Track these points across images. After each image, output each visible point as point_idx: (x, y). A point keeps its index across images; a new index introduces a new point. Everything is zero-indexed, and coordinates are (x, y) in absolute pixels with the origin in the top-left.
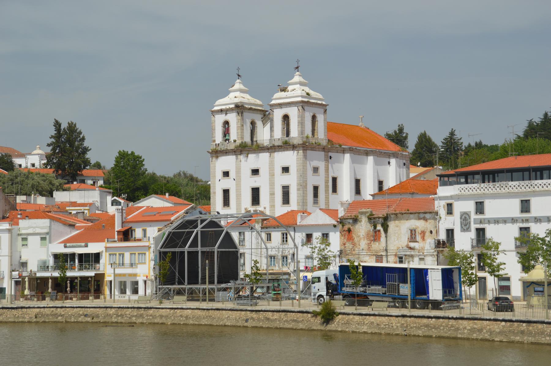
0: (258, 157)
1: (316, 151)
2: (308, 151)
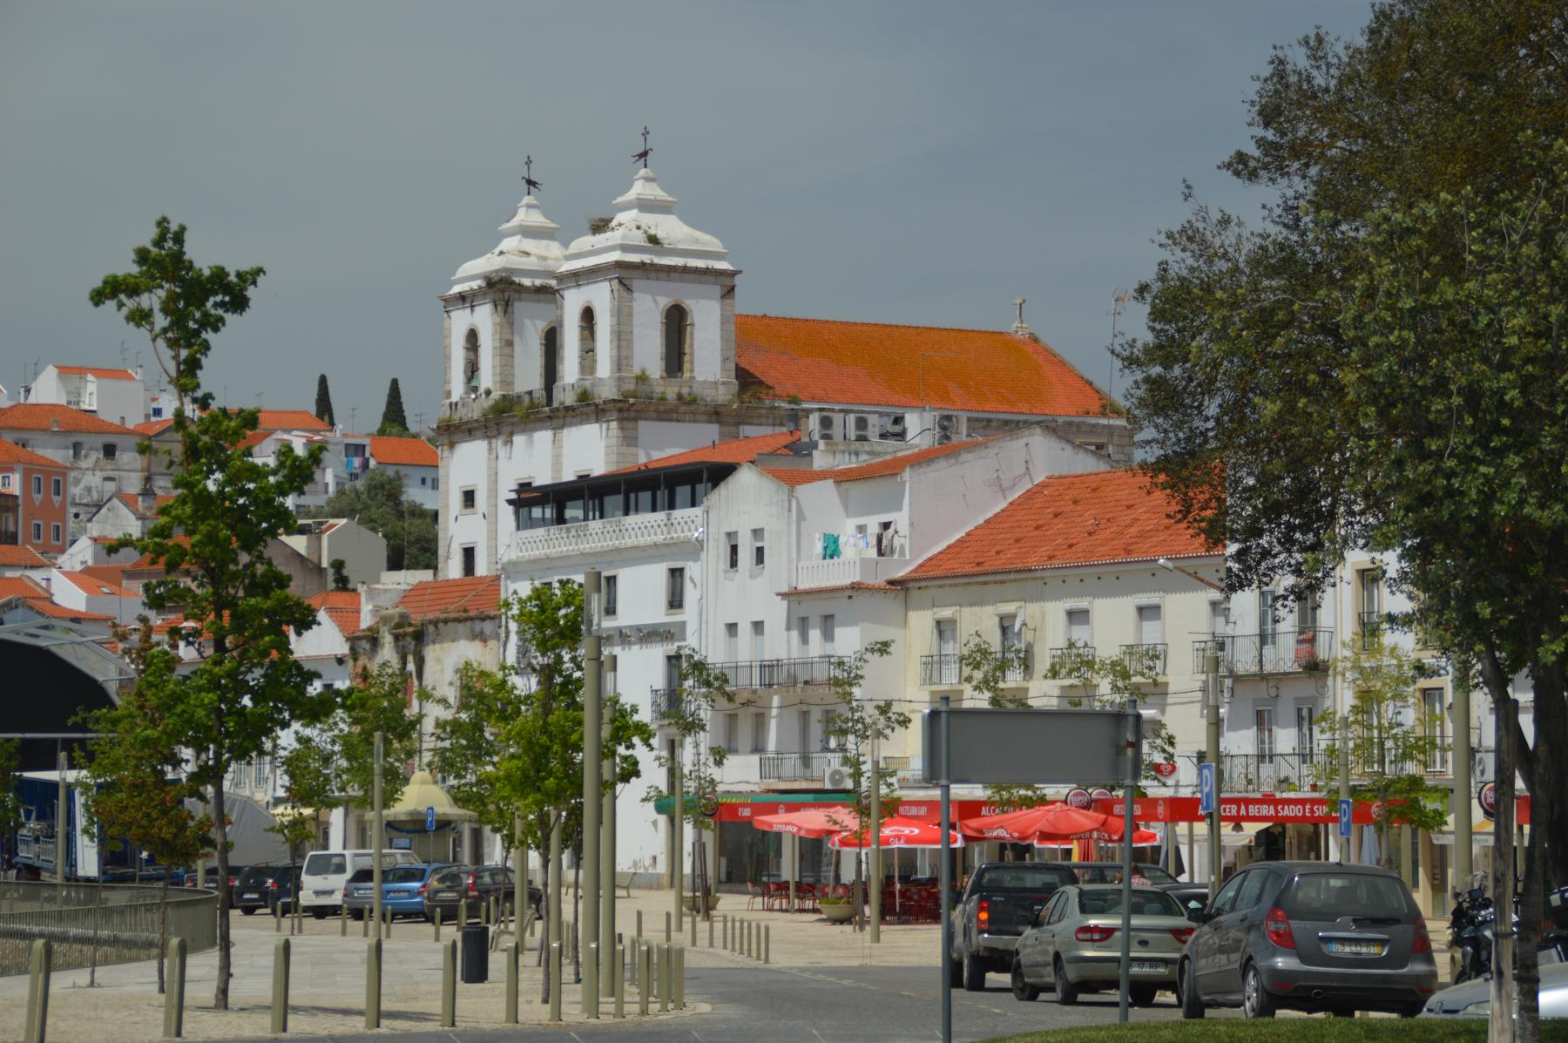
0: (532, 442)
1: (678, 421)
2: (642, 424)
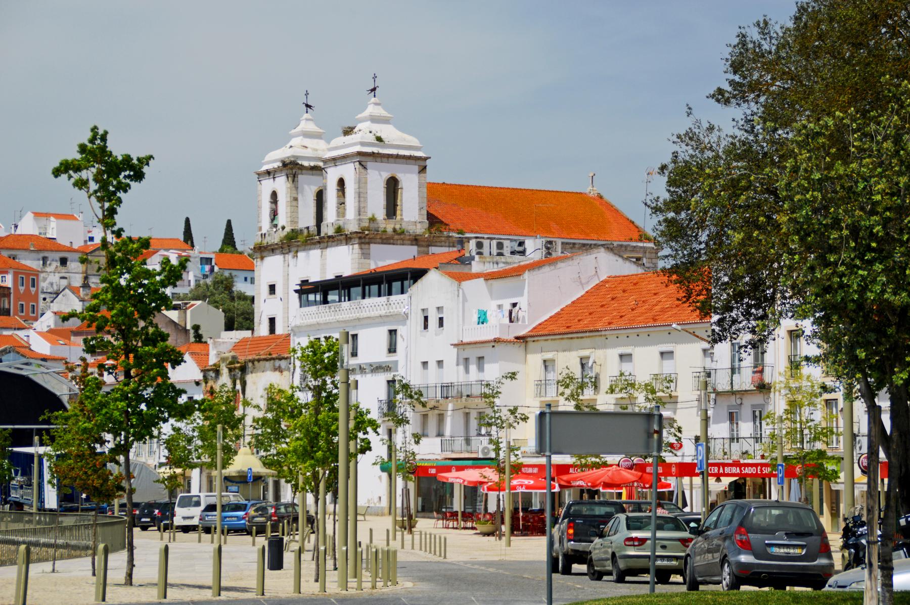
1: (394, 244)
2: (372, 246)
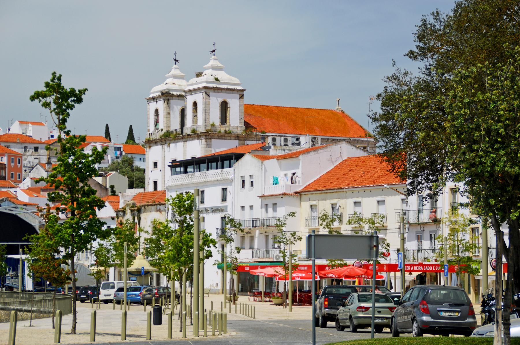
1: (225, 139)
2: (213, 140)
